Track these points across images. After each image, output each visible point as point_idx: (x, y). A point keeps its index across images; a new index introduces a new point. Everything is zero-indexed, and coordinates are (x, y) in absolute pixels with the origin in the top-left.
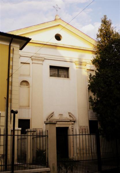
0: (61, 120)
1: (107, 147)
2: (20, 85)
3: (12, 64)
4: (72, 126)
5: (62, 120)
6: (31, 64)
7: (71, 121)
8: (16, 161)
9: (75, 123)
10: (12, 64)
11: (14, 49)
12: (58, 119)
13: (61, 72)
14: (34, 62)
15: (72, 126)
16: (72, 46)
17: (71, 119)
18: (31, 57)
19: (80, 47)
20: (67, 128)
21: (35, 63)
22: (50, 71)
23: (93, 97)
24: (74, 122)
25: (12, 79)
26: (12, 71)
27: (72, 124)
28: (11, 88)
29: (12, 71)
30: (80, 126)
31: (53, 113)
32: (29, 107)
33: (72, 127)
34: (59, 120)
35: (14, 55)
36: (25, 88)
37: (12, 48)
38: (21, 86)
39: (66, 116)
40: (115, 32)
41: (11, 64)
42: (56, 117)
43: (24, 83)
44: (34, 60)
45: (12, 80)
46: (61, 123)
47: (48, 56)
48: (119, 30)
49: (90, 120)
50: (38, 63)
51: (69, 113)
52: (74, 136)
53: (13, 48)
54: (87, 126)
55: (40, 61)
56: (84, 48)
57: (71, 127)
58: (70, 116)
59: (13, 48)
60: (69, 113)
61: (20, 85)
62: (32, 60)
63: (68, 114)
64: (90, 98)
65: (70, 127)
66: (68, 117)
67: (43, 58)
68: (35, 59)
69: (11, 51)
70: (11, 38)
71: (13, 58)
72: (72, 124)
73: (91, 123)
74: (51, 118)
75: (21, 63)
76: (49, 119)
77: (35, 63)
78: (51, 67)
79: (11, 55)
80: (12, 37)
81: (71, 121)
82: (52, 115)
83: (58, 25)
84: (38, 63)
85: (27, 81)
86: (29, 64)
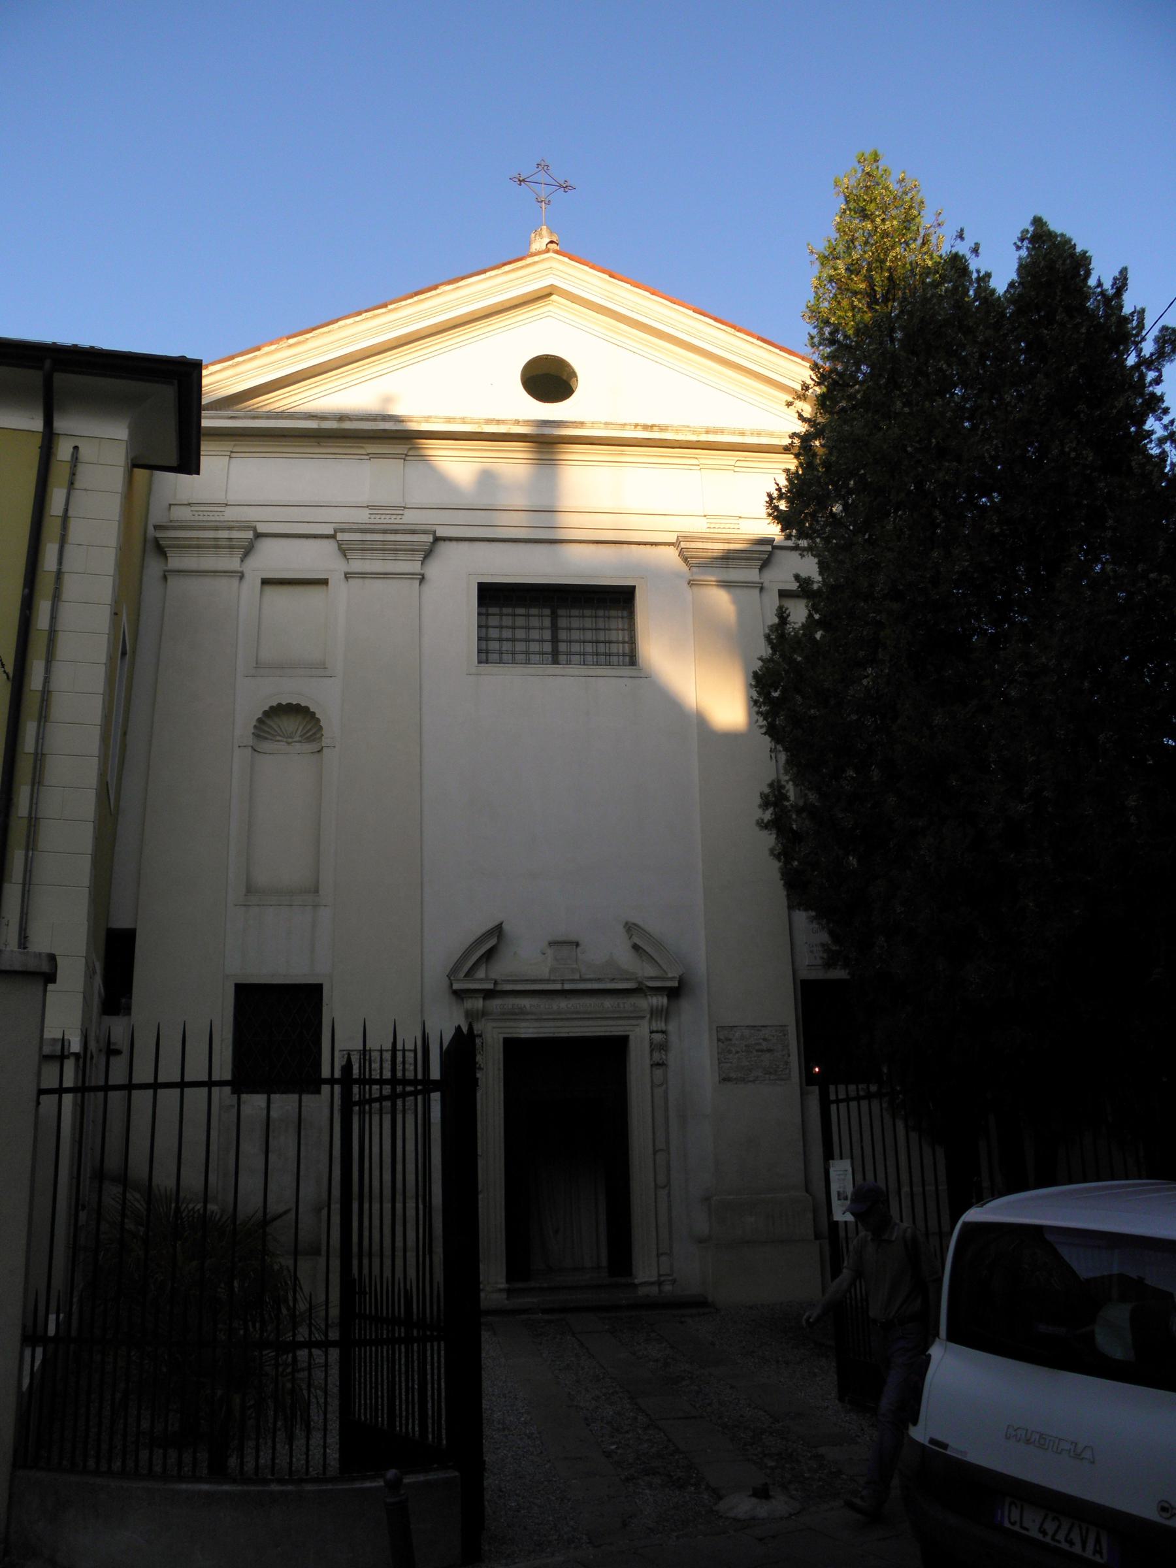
0: (563, 982)
1: (912, 1195)
2: (257, 736)
3: (60, 562)
4: (659, 1025)
5: (567, 987)
6: (336, 579)
7: (640, 990)
8: (164, 1320)
9: (685, 1005)
10: (60, 562)
11: (86, 452)
12: (545, 972)
13: (576, 623)
14: (357, 566)
15: (661, 1026)
16: (646, 428)
17: (649, 971)
18: (333, 537)
19: (716, 431)
20: (617, 1046)
21: (363, 575)
22: (479, 614)
23: (791, 790)
24: (675, 993)
25: (48, 670)
26: (53, 618)
27: (655, 1013)
28: (40, 738)
29: (53, 618)
30: (720, 1028)
31: (498, 931)
32: (317, 891)
33: (658, 1037)
34: (548, 981)
35: (76, 494)
36: (286, 765)
37: (63, 451)
38: (266, 746)
39: (608, 952)
40: (978, 272)
41: (49, 561)
42: (526, 958)
43: (290, 724)
44: (358, 555)
45: (47, 681)
46: (563, 1004)
47: (461, 518)
48: (961, 236)
49: (805, 974)
50: (385, 575)
51: (631, 928)
52: (215, 1090)
53: (76, 448)
54: (783, 1028)
55: (401, 555)
56: (742, 433)
57: (647, 1031)
58: (636, 947)
59: (76, 448)
60: (631, 928)
61: (250, 740)
62: (344, 551)
63: (621, 929)
64: (776, 788)
65: (640, 1035)
66: (625, 958)
67: (425, 532)
68: (366, 549)
69: (59, 474)
70: (54, 375)
71: (65, 517)
72: (655, 1013)
73: (811, 996)
74: (481, 974)
75: (266, 582)
76: (462, 975)
77: (363, 575)
78: (493, 596)
79: (57, 498)
80: (48, 364)
81: (640, 990)
82: (491, 945)
83: (543, 296)
84: (385, 575)
85: (313, 714)
86: (324, 582)
